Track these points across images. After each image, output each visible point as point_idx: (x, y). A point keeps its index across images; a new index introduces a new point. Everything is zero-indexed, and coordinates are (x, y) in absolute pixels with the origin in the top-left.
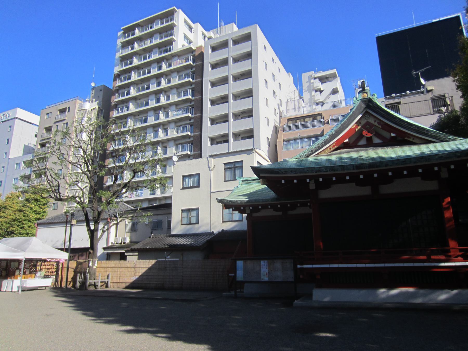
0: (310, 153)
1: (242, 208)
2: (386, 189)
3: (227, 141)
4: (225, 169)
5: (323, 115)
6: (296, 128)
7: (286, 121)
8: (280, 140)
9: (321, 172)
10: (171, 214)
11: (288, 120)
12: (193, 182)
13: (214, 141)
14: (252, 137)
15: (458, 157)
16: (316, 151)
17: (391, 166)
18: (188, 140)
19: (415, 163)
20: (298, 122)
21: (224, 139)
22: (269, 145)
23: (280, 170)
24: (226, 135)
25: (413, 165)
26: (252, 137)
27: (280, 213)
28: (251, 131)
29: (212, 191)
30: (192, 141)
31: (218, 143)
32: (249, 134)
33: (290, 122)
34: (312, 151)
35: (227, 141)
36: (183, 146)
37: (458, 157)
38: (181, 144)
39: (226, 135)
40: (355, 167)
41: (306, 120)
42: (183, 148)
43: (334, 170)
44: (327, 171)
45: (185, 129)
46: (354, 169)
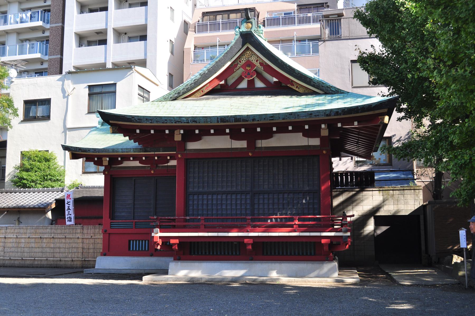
0: (176, 95)
1: (167, 132)
2: (262, 143)
3: (103, 42)
4: (89, 95)
5: (258, 9)
6: (215, 27)
7: (201, 15)
8: (190, 44)
9: (181, 123)
10: (5, 157)
11: (204, 14)
12: (40, 111)
13: (84, 40)
14: (143, 38)
15: (327, 115)
16: (184, 93)
17: (258, 121)
18: (40, 34)
19: (284, 119)
20: (219, 18)
21: (97, 39)
22: (172, 53)
23: (133, 117)
24: (103, 32)
25: (281, 121)
26: (143, 38)
27: (243, 144)
28: (144, 28)
29: (69, 125)
30: (48, 37)
31: (90, 43)
32: (140, 34)
33: (206, 17)
34: (179, 93)
35: (103, 42)
36: (33, 44)
37: (327, 115)
38: (29, 40)
39: (103, 32)
40: (219, 120)
41: (233, 16)
42: (33, 48)
43: (196, 122)
44: (188, 123)
45: (36, 15)
46: (218, 122)
